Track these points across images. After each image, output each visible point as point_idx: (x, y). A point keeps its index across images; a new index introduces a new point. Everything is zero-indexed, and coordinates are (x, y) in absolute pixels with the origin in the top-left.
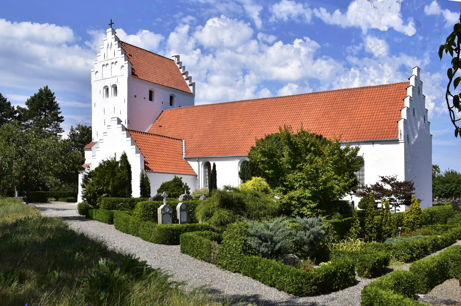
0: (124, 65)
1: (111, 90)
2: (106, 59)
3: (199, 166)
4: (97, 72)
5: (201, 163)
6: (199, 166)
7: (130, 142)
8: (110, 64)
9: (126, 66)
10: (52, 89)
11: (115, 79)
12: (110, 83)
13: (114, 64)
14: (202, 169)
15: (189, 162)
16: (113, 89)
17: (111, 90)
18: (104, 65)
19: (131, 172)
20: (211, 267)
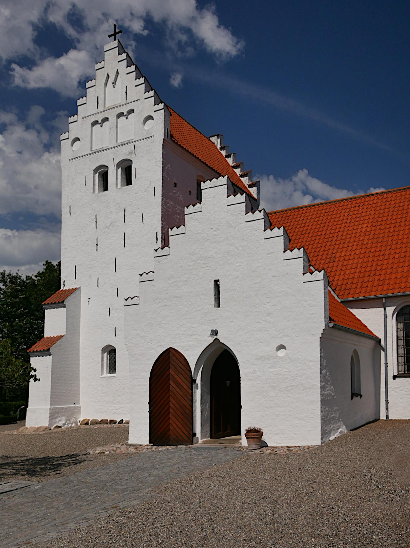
0: (153, 114)
1: (114, 176)
2: (101, 109)
3: (386, 316)
4: (77, 139)
5: (390, 310)
6: (386, 316)
7: (299, 265)
8: (112, 119)
9: (160, 117)
10: (218, 330)
11: (130, 147)
12: (110, 160)
13: (123, 118)
14: (392, 323)
15: (355, 312)
16: (120, 170)
17: (114, 176)
18: (96, 123)
19: (240, 407)
20: (406, 515)
